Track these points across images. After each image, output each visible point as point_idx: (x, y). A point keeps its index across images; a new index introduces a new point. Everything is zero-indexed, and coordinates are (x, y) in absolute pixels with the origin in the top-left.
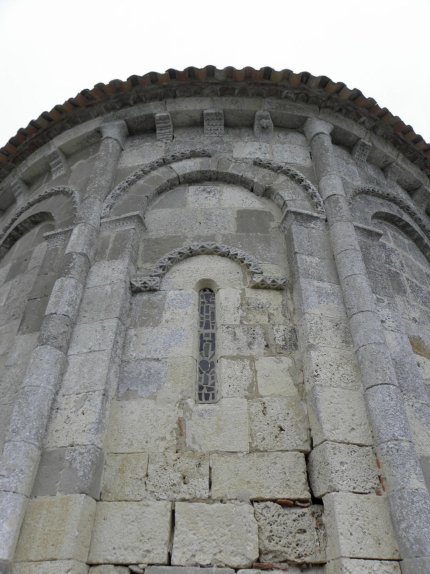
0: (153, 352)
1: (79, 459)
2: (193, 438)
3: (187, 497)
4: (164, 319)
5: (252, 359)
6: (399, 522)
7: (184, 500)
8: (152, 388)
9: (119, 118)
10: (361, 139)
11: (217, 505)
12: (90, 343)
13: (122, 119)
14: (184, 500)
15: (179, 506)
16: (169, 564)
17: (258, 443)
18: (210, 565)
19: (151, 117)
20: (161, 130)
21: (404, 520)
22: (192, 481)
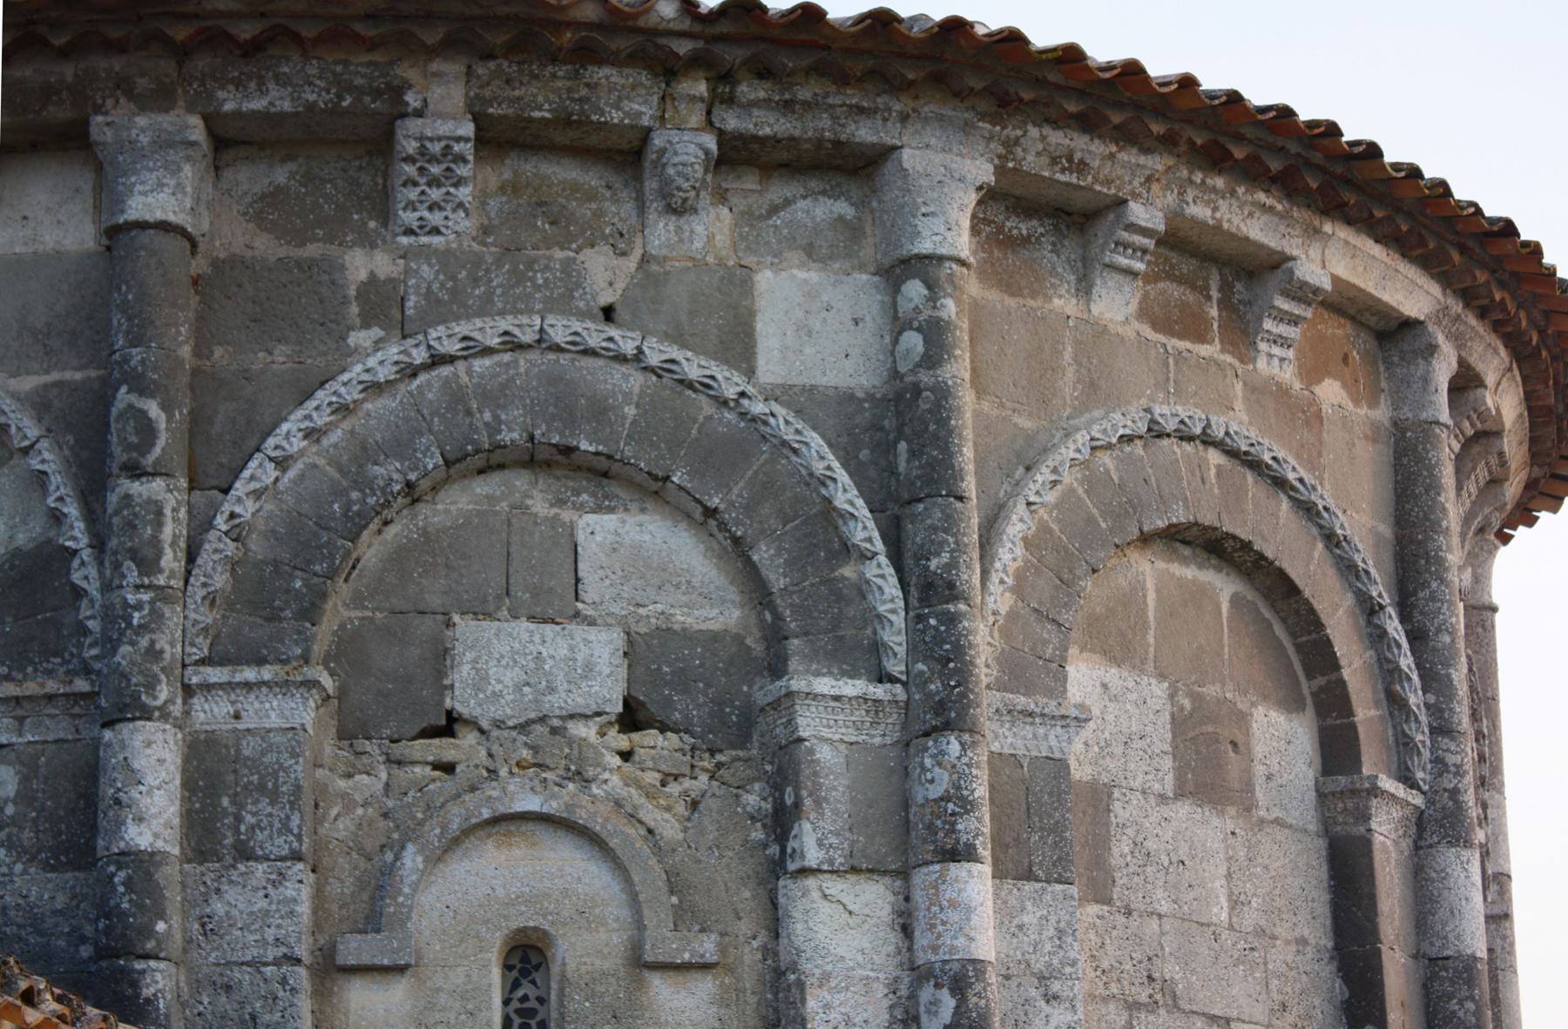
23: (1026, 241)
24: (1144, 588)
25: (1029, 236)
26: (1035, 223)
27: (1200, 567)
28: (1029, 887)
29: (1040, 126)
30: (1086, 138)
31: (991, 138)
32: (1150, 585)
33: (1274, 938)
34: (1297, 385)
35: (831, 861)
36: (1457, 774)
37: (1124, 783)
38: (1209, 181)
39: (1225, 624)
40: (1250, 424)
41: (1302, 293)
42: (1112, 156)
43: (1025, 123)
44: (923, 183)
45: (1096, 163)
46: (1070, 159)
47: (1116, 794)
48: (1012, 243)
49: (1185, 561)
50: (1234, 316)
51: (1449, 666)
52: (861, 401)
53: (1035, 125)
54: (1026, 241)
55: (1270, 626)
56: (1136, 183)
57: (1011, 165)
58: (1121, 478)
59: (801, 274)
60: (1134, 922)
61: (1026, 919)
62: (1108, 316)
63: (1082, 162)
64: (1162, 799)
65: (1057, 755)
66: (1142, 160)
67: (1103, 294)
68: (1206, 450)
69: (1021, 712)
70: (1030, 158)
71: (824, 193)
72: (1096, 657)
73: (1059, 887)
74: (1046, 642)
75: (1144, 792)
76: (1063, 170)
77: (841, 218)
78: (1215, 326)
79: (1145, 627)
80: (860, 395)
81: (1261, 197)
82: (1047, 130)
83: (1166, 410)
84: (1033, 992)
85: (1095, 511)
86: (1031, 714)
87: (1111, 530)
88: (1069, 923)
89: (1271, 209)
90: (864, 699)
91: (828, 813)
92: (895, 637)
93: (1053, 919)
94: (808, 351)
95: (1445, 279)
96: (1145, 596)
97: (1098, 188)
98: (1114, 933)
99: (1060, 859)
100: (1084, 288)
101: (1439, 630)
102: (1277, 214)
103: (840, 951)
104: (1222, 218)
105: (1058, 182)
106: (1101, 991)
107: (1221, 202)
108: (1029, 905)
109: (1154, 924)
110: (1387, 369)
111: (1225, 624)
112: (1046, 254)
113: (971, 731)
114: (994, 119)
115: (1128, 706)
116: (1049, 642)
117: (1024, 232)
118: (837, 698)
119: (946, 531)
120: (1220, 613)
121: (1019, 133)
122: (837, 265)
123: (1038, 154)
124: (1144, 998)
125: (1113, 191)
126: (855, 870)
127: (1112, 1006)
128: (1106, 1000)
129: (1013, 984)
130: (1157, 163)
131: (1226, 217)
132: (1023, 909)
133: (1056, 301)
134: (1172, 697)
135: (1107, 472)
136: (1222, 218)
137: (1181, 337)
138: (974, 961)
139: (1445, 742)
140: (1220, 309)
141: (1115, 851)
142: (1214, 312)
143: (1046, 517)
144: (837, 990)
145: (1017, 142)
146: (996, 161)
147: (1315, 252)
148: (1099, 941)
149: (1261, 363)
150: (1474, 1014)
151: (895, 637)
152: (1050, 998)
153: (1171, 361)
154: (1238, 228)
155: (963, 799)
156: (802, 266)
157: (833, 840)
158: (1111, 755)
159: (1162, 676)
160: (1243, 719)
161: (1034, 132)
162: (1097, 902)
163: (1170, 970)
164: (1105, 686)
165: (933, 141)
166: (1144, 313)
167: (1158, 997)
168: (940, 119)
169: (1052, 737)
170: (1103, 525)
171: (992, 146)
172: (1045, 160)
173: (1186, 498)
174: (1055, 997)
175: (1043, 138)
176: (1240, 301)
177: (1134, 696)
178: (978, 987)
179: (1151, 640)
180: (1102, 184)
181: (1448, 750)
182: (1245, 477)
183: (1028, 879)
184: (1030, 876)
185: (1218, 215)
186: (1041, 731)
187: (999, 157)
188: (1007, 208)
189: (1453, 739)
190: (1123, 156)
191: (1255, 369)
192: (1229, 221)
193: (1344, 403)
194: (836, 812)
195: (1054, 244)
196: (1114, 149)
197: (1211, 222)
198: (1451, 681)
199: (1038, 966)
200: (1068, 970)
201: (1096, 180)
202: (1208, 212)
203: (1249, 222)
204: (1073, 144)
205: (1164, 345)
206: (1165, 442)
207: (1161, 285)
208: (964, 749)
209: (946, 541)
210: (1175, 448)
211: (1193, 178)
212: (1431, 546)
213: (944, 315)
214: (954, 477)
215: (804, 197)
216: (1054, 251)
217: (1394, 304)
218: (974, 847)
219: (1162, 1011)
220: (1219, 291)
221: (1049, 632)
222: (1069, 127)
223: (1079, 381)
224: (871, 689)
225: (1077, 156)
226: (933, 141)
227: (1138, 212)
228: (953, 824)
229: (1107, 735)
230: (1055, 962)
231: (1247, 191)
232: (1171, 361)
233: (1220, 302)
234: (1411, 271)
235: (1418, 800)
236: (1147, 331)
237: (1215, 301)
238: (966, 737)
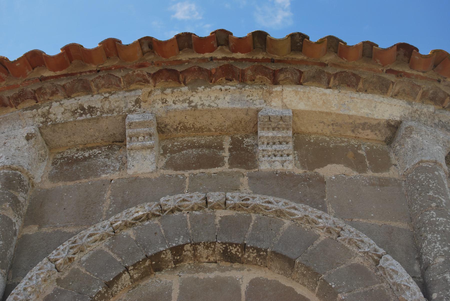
24: (170, 290)
30: (89, 97)
31: (34, 116)
39: (243, 293)
46: (82, 108)
63: (90, 107)
76: (81, 115)
120: (240, 295)
121: (47, 108)
131: (199, 104)
133: (104, 176)
153: (187, 180)
171: (36, 119)
201: (102, 112)
225: (86, 106)
232: (187, 180)
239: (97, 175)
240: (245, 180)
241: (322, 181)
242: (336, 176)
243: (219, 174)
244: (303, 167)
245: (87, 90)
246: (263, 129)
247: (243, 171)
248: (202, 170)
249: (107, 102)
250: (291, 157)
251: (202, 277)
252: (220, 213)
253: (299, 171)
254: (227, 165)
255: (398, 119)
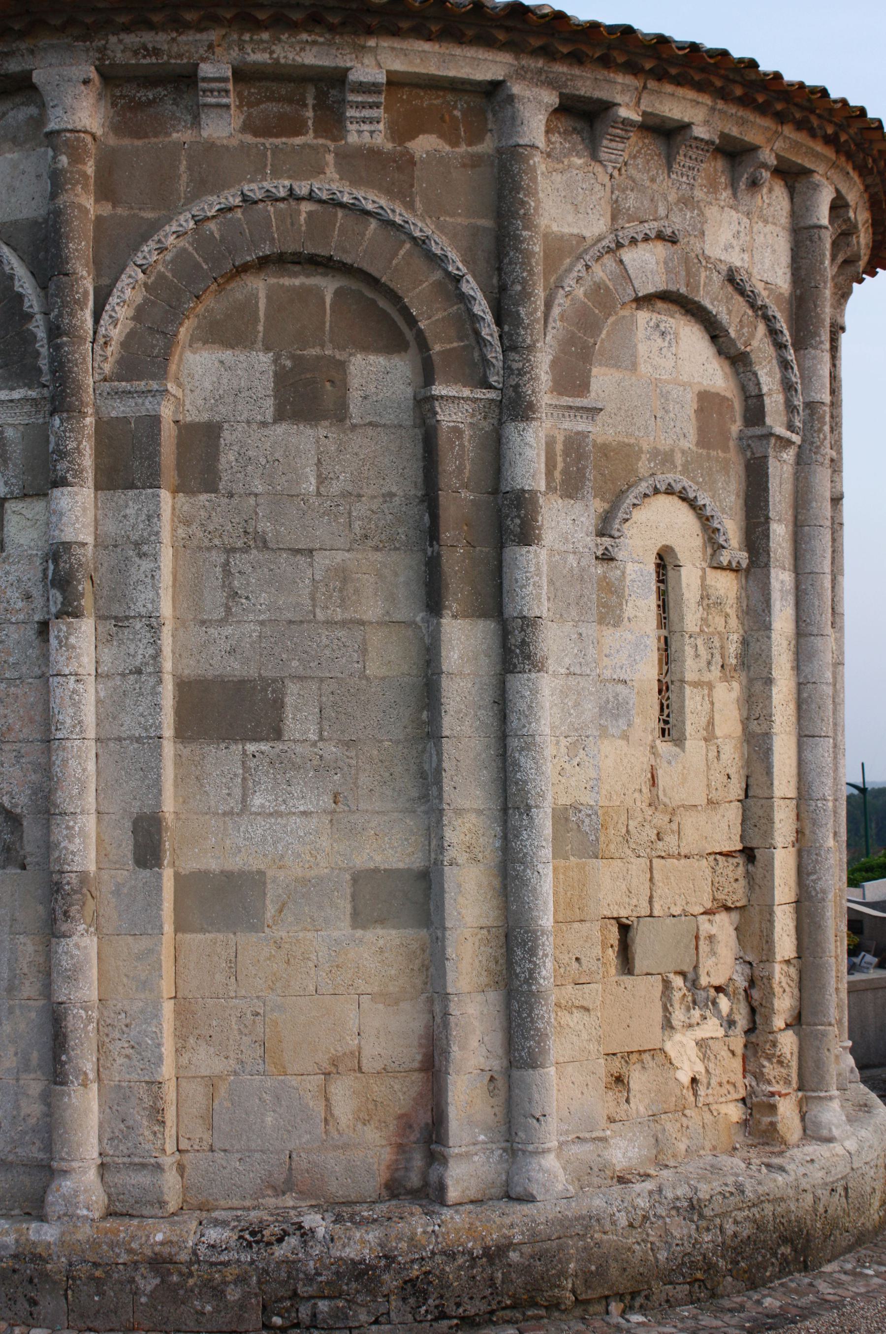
0: (618, 670)
1: (587, 821)
2: (664, 790)
3: (663, 854)
4: (626, 615)
5: (710, 686)
6: (809, 874)
7: (659, 857)
8: (622, 723)
9: (551, 83)
10: (815, 175)
11: (683, 861)
12: (567, 659)
13: (554, 88)
14: (659, 857)
15: (655, 861)
16: (651, 916)
17: (714, 795)
18: (680, 915)
19: (608, 106)
20: (611, 140)
21: (815, 873)
22: (667, 838)
23: (150, 103)
24: (257, 297)
25: (154, 98)
26: (159, 89)
27: (308, 276)
28: (131, 493)
29: (117, 34)
30: (153, 33)
31: (88, 50)
32: (262, 295)
33: (359, 496)
34: (389, 146)
35: (12, 493)
36: (519, 375)
37: (232, 419)
38: (255, 37)
39: (328, 307)
40: (341, 179)
41: (363, 88)
42: (174, 40)
43: (107, 35)
44: (49, 88)
45: (166, 47)
46: (146, 49)
47: (226, 426)
48: (139, 106)
49: (295, 275)
50: (328, 113)
51: (519, 305)
52: (41, 223)
53: (113, 34)
54: (150, 103)
55: (374, 302)
56: (201, 51)
57: (107, 62)
58: (222, 236)
59: (9, 156)
60: (235, 501)
61: (128, 511)
62: (215, 135)
63: (154, 48)
64: (264, 424)
65: (153, 413)
66: (198, 36)
67: (209, 122)
68: (298, 205)
69: (123, 392)
70: (119, 55)
71: (23, 104)
72: (216, 346)
73: (149, 491)
74: (153, 347)
75: (248, 422)
76: (144, 57)
77: (31, 117)
78: (310, 123)
79: (256, 320)
80: (40, 220)
81: (304, 36)
82: (123, 36)
83: (254, 186)
84: (131, 553)
85: (200, 260)
86: (130, 392)
87: (210, 269)
88: (155, 512)
89: (314, 43)
90: (26, 399)
91: (11, 466)
92: (43, 364)
93: (145, 510)
94: (13, 200)
95: (503, 47)
96: (257, 303)
97: (173, 61)
98: (219, 509)
99: (151, 474)
100: (196, 122)
101: (513, 283)
102: (322, 44)
103: (22, 541)
104: (278, 58)
105: (142, 65)
106: (206, 543)
107: (274, 47)
108: (130, 503)
109: (252, 501)
110: (494, 115)
111: (328, 307)
112: (168, 107)
113: (67, 411)
114: (85, 38)
115: (239, 372)
116: (156, 346)
117: (151, 97)
118: (12, 401)
119: (57, 296)
120: (324, 303)
121: (103, 42)
122: (28, 146)
123: (123, 51)
124: (240, 544)
125: (185, 61)
126: (25, 495)
127: (214, 553)
128: (209, 549)
129: (119, 550)
130: (213, 35)
131: (282, 55)
132: (127, 506)
133: (175, 135)
134: (275, 361)
135: (212, 233)
136: (278, 58)
137: (277, 136)
138: (63, 543)
139: (513, 355)
140: (314, 110)
141: (223, 460)
142: (310, 114)
143: (162, 270)
144: (13, 563)
145: (105, 48)
146: (97, 63)
147: (368, 60)
148: (207, 515)
149: (353, 138)
150: (519, 526)
151: (43, 364)
152: (142, 555)
153: (269, 153)
154: (294, 60)
155: (60, 451)
156: (11, 151)
157: (14, 481)
158: (224, 404)
159: (267, 349)
160: (342, 366)
161: (113, 39)
162: (207, 492)
163: (265, 526)
164: (222, 362)
165: (54, 61)
166: (248, 127)
167: (251, 543)
168: (52, 46)
169: (147, 403)
170: (205, 267)
171: (91, 54)
172: (129, 54)
173: (273, 239)
174: (145, 554)
175: (120, 41)
176: (334, 102)
177: (245, 365)
178: (65, 557)
179: (261, 328)
180: (176, 58)
181: (514, 360)
182: (336, 215)
183: (131, 488)
184: (133, 486)
185: (275, 56)
186: (140, 401)
187: (99, 59)
188: (138, 85)
189: (518, 353)
190: (183, 38)
191: (346, 143)
192: (285, 57)
193: (439, 148)
194: (15, 465)
195: (174, 99)
196: (174, 35)
197: (269, 61)
198: (519, 315)
199: (135, 537)
200: (153, 538)
201: (170, 57)
202: (267, 56)
203: (302, 54)
204: (142, 40)
205: (263, 144)
206: (261, 205)
207: (262, 106)
208: (62, 423)
209: (56, 302)
210: (269, 208)
211: (243, 38)
212: (511, 228)
213: (60, 166)
214: (62, 263)
215: (12, 109)
216: (175, 103)
217: (465, 76)
218: (66, 478)
219: (254, 551)
220: (315, 99)
221: (158, 340)
222: (139, 30)
223: (191, 181)
224: (30, 393)
225: (150, 46)
226: (54, 61)
227: (206, 69)
228: (55, 466)
229: (221, 392)
230: (145, 534)
231: (290, 36)
232: (269, 153)
233: (314, 106)
234: (471, 52)
235: (492, 395)
236: (249, 139)
237: (310, 107)
238: (65, 415)
239: (166, 133)
240: (330, 158)
241: (408, 162)
242: (427, 153)
243: (303, 146)
244: (394, 141)
245: (151, 26)
246: (352, 91)
247: (329, 143)
248: (284, 140)
249: (175, 45)
250: (381, 126)
251: (287, 283)
252: (306, 207)
253: (389, 146)
254: (311, 133)
255: (501, 78)
